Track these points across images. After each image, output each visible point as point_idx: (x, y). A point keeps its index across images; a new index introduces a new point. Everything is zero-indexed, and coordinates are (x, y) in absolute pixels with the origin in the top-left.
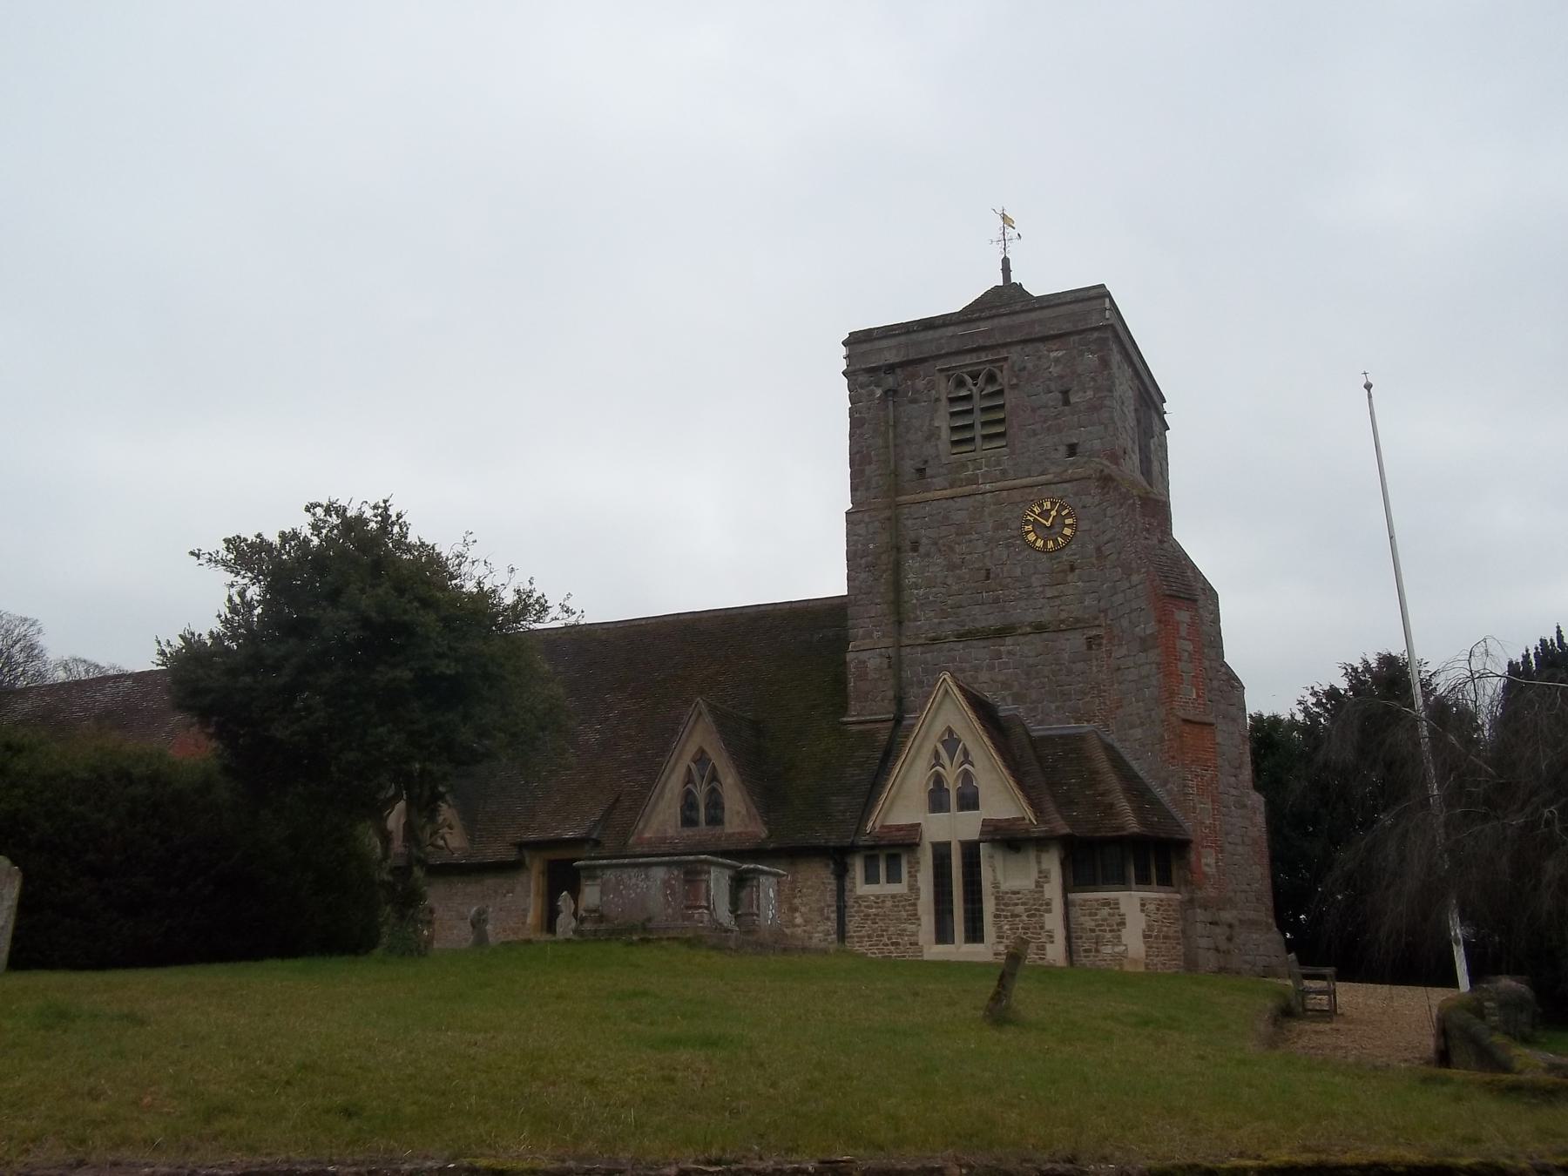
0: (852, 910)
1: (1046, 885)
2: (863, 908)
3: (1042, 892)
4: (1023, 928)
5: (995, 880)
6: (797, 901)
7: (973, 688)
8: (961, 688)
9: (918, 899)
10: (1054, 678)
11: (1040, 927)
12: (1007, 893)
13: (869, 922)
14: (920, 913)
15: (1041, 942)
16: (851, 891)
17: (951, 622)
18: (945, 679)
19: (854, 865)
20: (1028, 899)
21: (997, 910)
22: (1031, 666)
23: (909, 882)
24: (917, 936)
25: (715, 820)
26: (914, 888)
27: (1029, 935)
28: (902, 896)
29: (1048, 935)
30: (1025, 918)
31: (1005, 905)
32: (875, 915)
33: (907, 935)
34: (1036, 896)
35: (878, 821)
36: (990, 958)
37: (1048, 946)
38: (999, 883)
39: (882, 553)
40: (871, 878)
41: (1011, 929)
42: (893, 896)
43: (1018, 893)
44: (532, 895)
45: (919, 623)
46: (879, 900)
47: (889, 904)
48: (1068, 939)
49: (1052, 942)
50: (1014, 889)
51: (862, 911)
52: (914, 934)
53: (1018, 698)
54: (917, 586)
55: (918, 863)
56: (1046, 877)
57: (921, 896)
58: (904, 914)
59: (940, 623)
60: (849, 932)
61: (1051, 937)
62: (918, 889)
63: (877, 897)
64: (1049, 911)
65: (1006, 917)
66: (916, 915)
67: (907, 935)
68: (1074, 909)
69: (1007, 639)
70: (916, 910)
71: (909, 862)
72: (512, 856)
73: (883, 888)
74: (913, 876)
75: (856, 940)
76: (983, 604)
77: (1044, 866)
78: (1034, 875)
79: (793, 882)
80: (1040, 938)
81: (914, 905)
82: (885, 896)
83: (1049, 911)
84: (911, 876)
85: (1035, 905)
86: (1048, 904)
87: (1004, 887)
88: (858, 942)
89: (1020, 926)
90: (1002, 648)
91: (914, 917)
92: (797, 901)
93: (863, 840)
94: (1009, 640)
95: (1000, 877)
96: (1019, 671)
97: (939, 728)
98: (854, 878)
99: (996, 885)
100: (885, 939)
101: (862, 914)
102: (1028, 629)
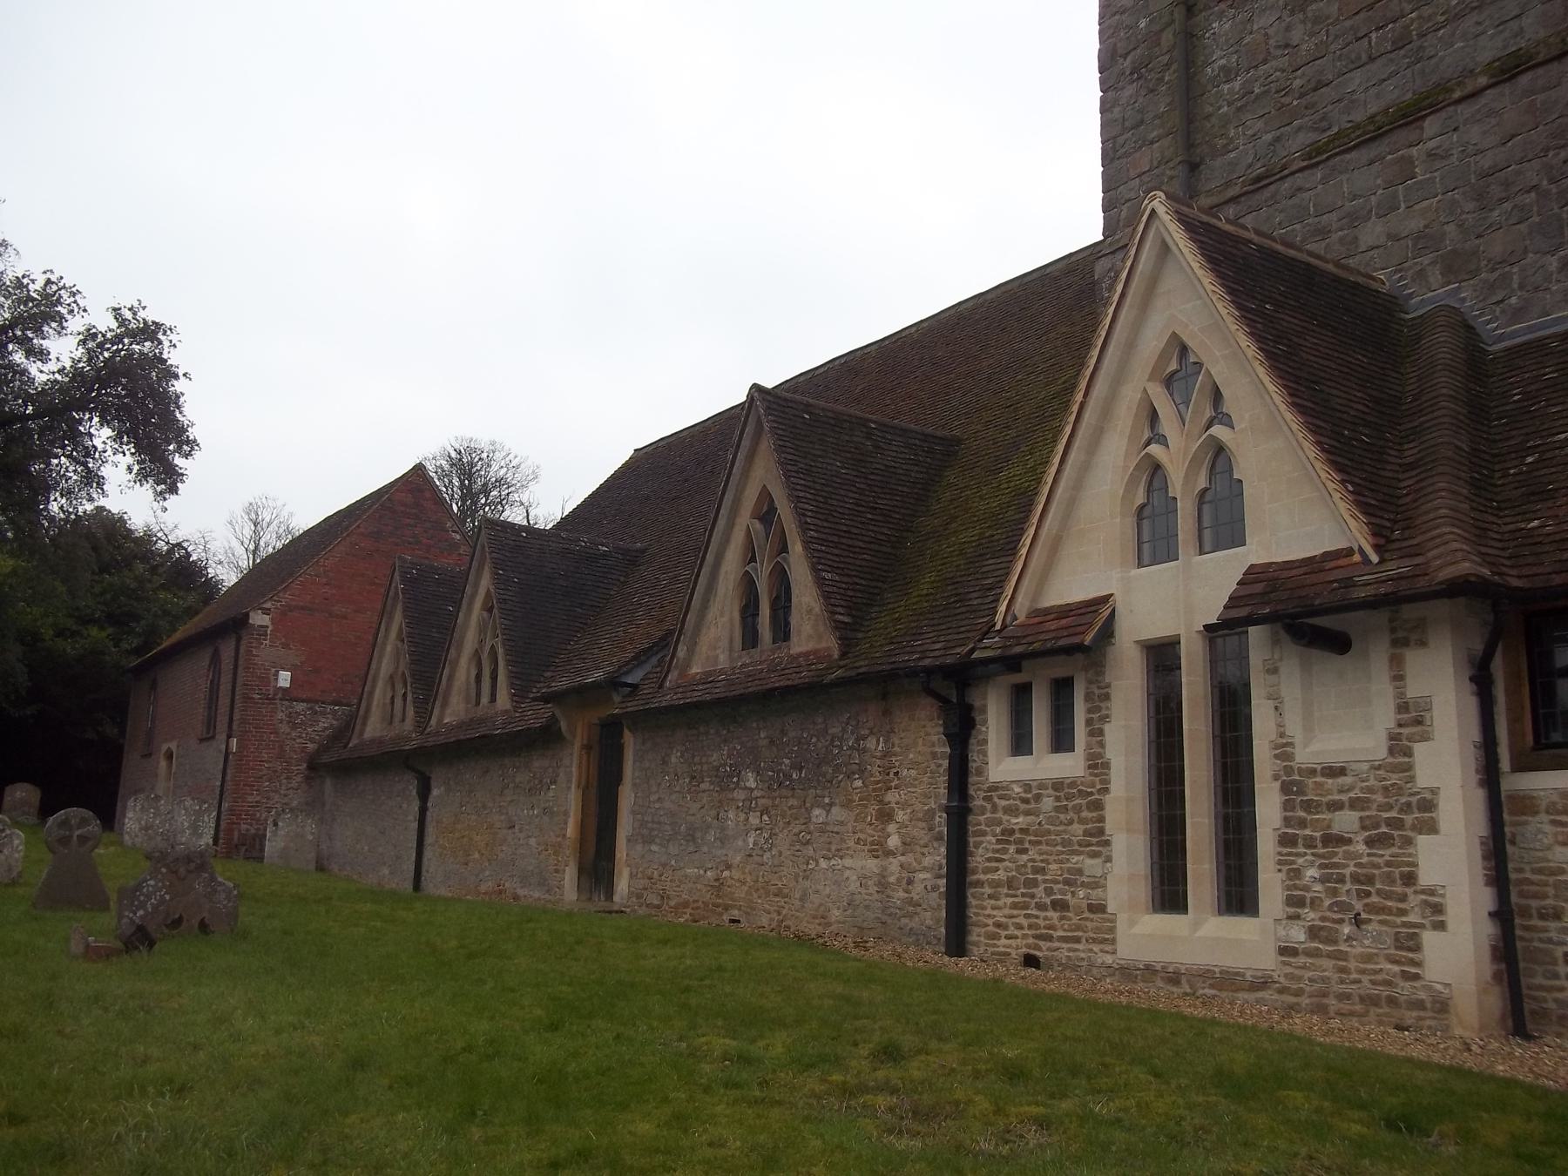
0: (982, 818)
1: (1419, 749)
2: (999, 815)
3: (1409, 767)
4: (1356, 879)
5: (1282, 735)
6: (891, 797)
7: (1346, 268)
8: (1193, 228)
9: (1106, 790)
10: (1554, 189)
11: (1402, 876)
12: (1313, 772)
13: (1012, 849)
14: (1109, 827)
15: (1405, 924)
16: (980, 772)
17: (1300, 129)
18: (1153, 210)
19: (984, 710)
20: (1370, 790)
21: (1287, 821)
22: (1485, 175)
23: (1089, 746)
24: (1104, 886)
25: (782, 631)
26: (1097, 764)
27: (1374, 899)
28: (1073, 784)
29: (1425, 902)
30: (1362, 848)
31: (1308, 806)
32: (1021, 830)
33: (1083, 885)
34: (1394, 778)
35: (1020, 598)
36: (1268, 961)
37: (1429, 938)
38: (1291, 744)
39: (1162, 31)
40: (1021, 744)
41: (1323, 880)
42: (1058, 785)
43: (1342, 771)
44: (573, 786)
45: (1232, 155)
46: (1032, 791)
47: (1048, 803)
48: (1503, 915)
49: (1440, 926)
50: (1335, 760)
51: (1000, 823)
52: (1097, 884)
53: (1456, 266)
54: (1228, 74)
55: (1107, 697)
56: (1419, 722)
57: (1113, 787)
58: (1078, 829)
59: (1277, 139)
60: (974, 872)
61: (1438, 909)
62: (1107, 765)
63: (1027, 787)
64: (1431, 828)
65: (1310, 843)
66: (1101, 832)
67: (1083, 885)
68: (980, 897)
69: (1427, 123)
70: (1102, 819)
71: (1088, 697)
72: (534, 716)
73: (1046, 765)
74: (1096, 733)
75: (987, 890)
76: (1372, 59)
77: (1413, 690)
78: (1384, 717)
79: (886, 755)
80: (1403, 912)
81: (1098, 806)
82: (1042, 786)
83: (1431, 828)
84: (1091, 734)
85: (1390, 807)
86: (1428, 805)
87: (1305, 756)
88: (990, 897)
89: (1347, 872)
90: (1414, 151)
91: (1097, 839)
92: (891, 797)
93: (989, 648)
94: (1431, 125)
95: (1294, 729)
96: (1456, 195)
97: (1152, 342)
98: (985, 742)
99: (1283, 751)
100: (1039, 891)
101: (998, 830)
102: (1483, 81)
